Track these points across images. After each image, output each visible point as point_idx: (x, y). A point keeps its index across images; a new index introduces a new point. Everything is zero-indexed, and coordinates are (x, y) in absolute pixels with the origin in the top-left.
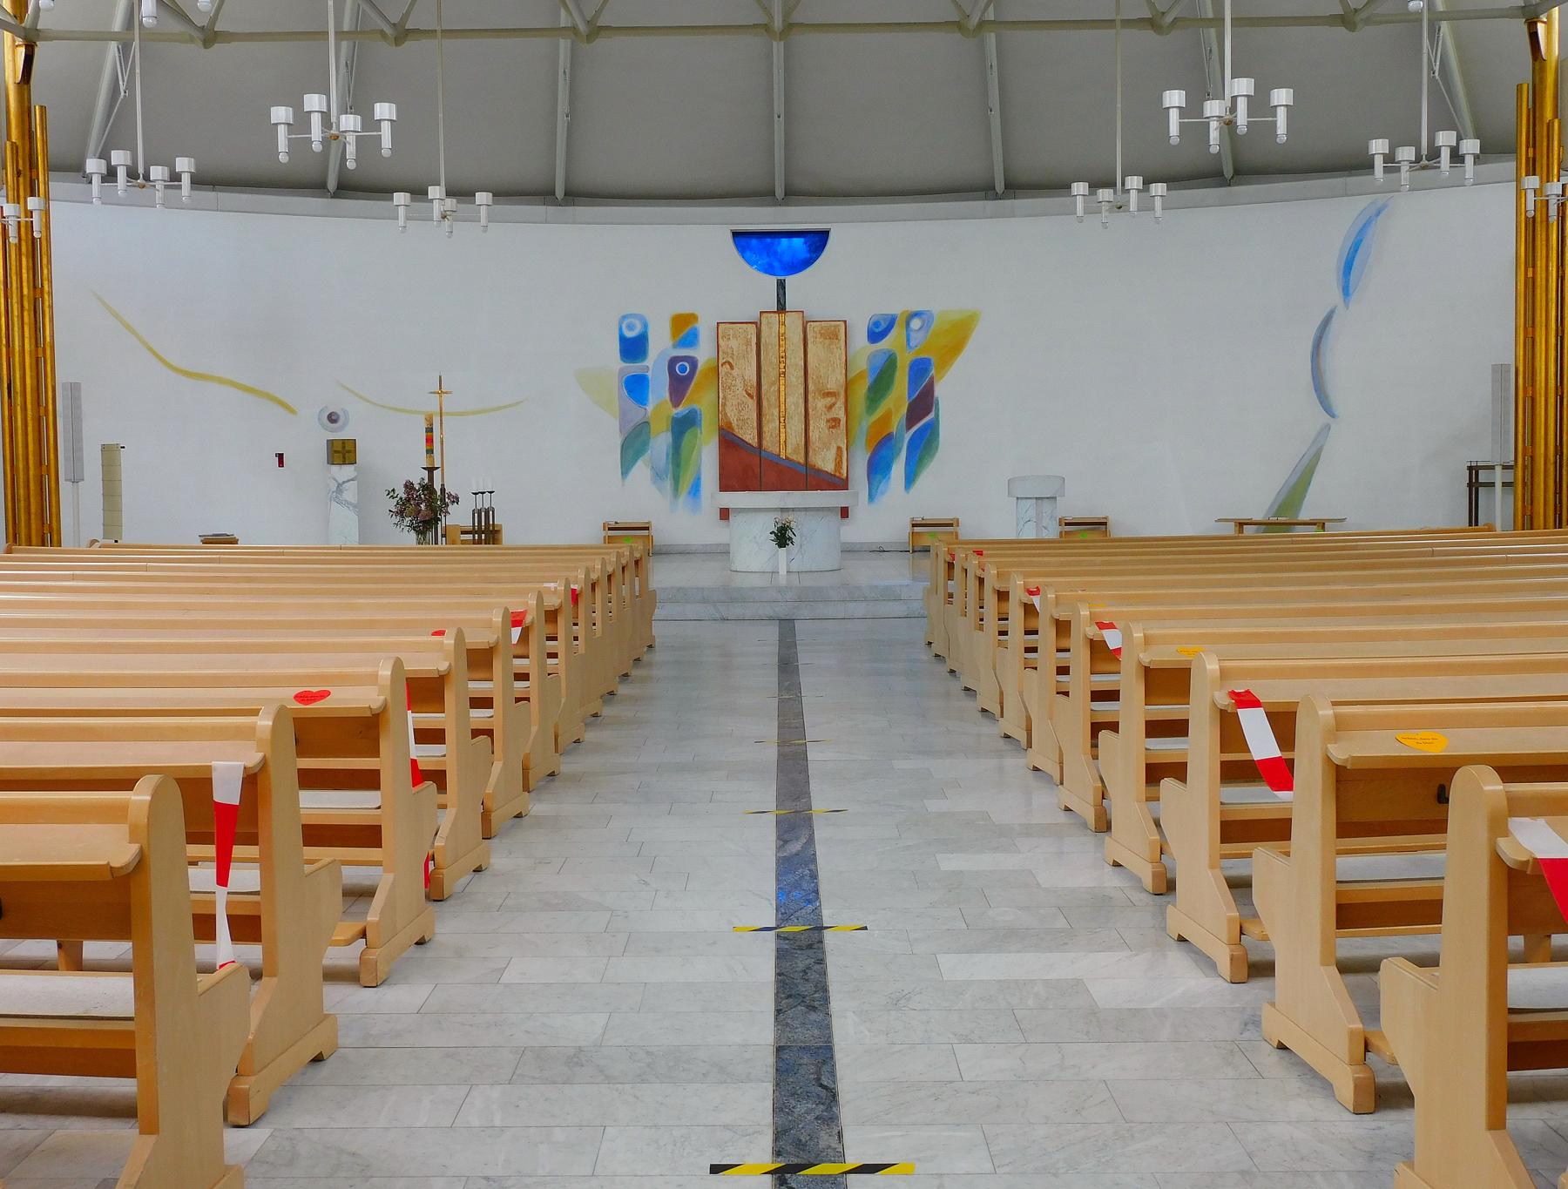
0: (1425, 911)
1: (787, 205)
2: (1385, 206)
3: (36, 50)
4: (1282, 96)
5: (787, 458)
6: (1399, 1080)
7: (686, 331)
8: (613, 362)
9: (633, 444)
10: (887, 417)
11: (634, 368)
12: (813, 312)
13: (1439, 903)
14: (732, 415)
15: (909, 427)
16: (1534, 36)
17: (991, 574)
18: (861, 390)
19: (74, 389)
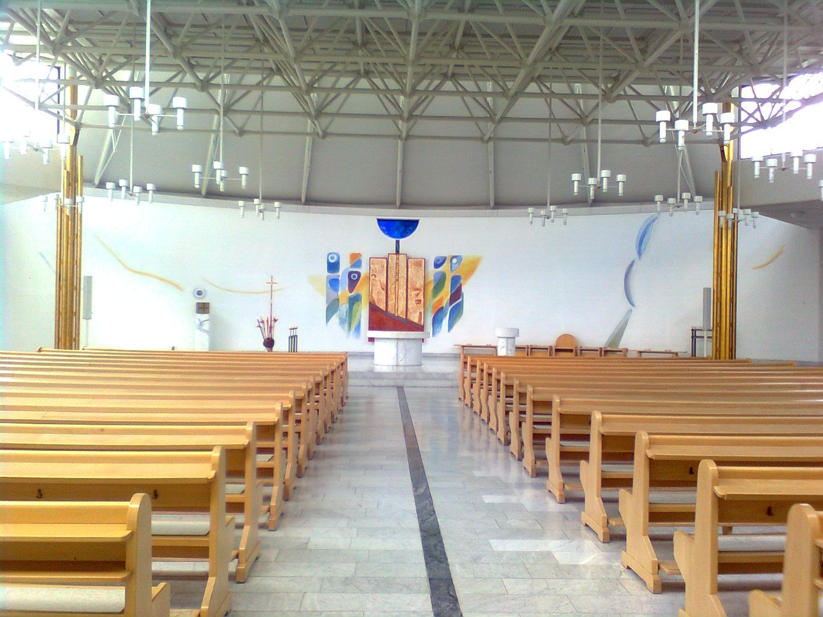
0: (688, 517)
1: (401, 208)
2: (656, 218)
3: (81, 131)
4: (620, 177)
5: (398, 316)
6: (678, 577)
7: (356, 260)
8: (324, 272)
9: (332, 308)
10: (441, 300)
11: (333, 275)
12: (411, 254)
13: (694, 514)
14: (375, 297)
15: (451, 304)
16: (722, 151)
17: (485, 367)
18: (431, 287)
19: (89, 279)
